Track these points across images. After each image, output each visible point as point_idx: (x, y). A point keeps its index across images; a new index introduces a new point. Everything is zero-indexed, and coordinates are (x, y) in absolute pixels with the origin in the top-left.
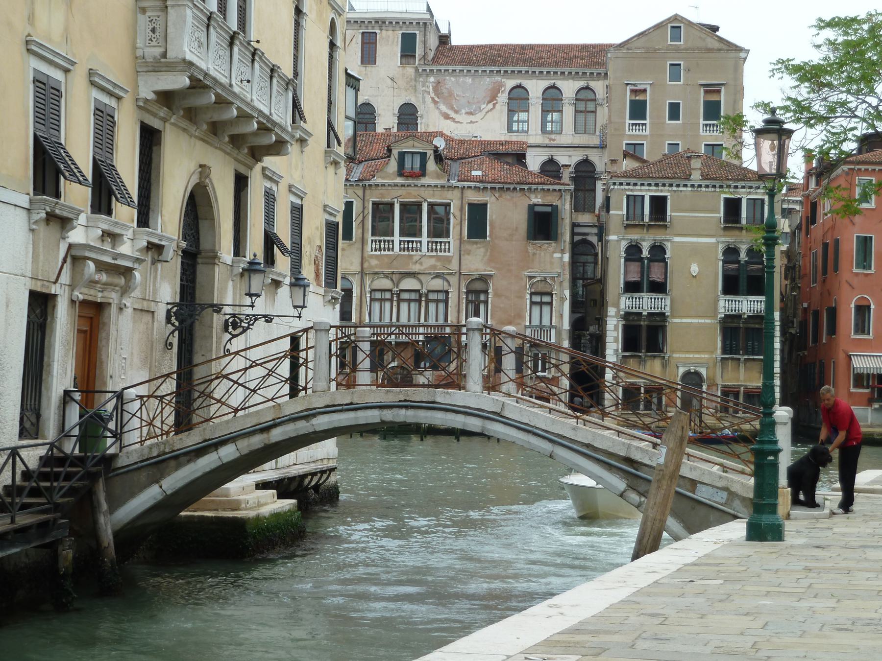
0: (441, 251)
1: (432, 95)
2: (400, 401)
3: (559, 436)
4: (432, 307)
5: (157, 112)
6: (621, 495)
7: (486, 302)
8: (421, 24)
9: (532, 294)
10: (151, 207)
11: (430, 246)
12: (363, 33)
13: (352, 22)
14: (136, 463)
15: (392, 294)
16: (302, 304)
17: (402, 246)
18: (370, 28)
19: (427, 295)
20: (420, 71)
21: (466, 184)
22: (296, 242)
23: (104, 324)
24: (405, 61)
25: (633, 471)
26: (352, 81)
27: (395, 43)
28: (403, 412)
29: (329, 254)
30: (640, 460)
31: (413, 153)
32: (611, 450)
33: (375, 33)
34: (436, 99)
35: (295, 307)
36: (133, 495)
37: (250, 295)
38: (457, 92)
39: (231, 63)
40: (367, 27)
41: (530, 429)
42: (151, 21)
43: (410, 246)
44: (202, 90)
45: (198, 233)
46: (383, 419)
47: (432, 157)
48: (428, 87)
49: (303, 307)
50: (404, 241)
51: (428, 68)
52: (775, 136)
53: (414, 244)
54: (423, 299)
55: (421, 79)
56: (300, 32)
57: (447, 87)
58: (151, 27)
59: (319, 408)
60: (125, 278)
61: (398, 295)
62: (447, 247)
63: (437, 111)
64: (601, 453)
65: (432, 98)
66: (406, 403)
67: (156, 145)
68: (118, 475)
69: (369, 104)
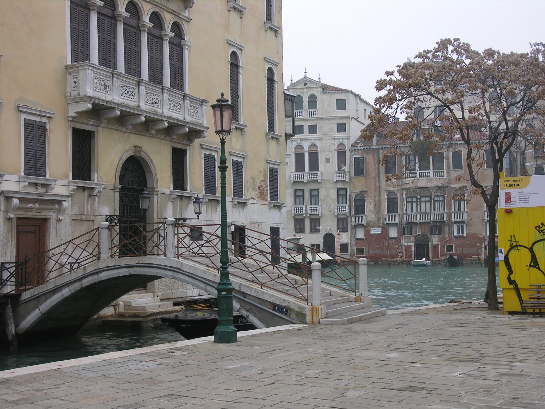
0: (440, 176)
2: (136, 264)
3: (207, 279)
5: (88, 122)
9: (406, 199)
10: (92, 169)
14: (29, 298)
15: (417, 199)
17: (421, 175)
22: (236, 179)
23: (48, 228)
25: (243, 298)
26: (288, 97)
28: (138, 269)
29: (271, 184)
30: (246, 292)
35: (196, 213)
36: (28, 314)
39: (139, 95)
41: (194, 276)
42: (73, 78)
44: (112, 109)
45: (146, 179)
49: (200, 213)
53: (427, 173)
56: (239, 76)
58: (74, 81)
59: (102, 268)
60: (59, 205)
61: (420, 199)
62: (443, 174)
66: (139, 265)
67: (93, 138)
68: (22, 304)
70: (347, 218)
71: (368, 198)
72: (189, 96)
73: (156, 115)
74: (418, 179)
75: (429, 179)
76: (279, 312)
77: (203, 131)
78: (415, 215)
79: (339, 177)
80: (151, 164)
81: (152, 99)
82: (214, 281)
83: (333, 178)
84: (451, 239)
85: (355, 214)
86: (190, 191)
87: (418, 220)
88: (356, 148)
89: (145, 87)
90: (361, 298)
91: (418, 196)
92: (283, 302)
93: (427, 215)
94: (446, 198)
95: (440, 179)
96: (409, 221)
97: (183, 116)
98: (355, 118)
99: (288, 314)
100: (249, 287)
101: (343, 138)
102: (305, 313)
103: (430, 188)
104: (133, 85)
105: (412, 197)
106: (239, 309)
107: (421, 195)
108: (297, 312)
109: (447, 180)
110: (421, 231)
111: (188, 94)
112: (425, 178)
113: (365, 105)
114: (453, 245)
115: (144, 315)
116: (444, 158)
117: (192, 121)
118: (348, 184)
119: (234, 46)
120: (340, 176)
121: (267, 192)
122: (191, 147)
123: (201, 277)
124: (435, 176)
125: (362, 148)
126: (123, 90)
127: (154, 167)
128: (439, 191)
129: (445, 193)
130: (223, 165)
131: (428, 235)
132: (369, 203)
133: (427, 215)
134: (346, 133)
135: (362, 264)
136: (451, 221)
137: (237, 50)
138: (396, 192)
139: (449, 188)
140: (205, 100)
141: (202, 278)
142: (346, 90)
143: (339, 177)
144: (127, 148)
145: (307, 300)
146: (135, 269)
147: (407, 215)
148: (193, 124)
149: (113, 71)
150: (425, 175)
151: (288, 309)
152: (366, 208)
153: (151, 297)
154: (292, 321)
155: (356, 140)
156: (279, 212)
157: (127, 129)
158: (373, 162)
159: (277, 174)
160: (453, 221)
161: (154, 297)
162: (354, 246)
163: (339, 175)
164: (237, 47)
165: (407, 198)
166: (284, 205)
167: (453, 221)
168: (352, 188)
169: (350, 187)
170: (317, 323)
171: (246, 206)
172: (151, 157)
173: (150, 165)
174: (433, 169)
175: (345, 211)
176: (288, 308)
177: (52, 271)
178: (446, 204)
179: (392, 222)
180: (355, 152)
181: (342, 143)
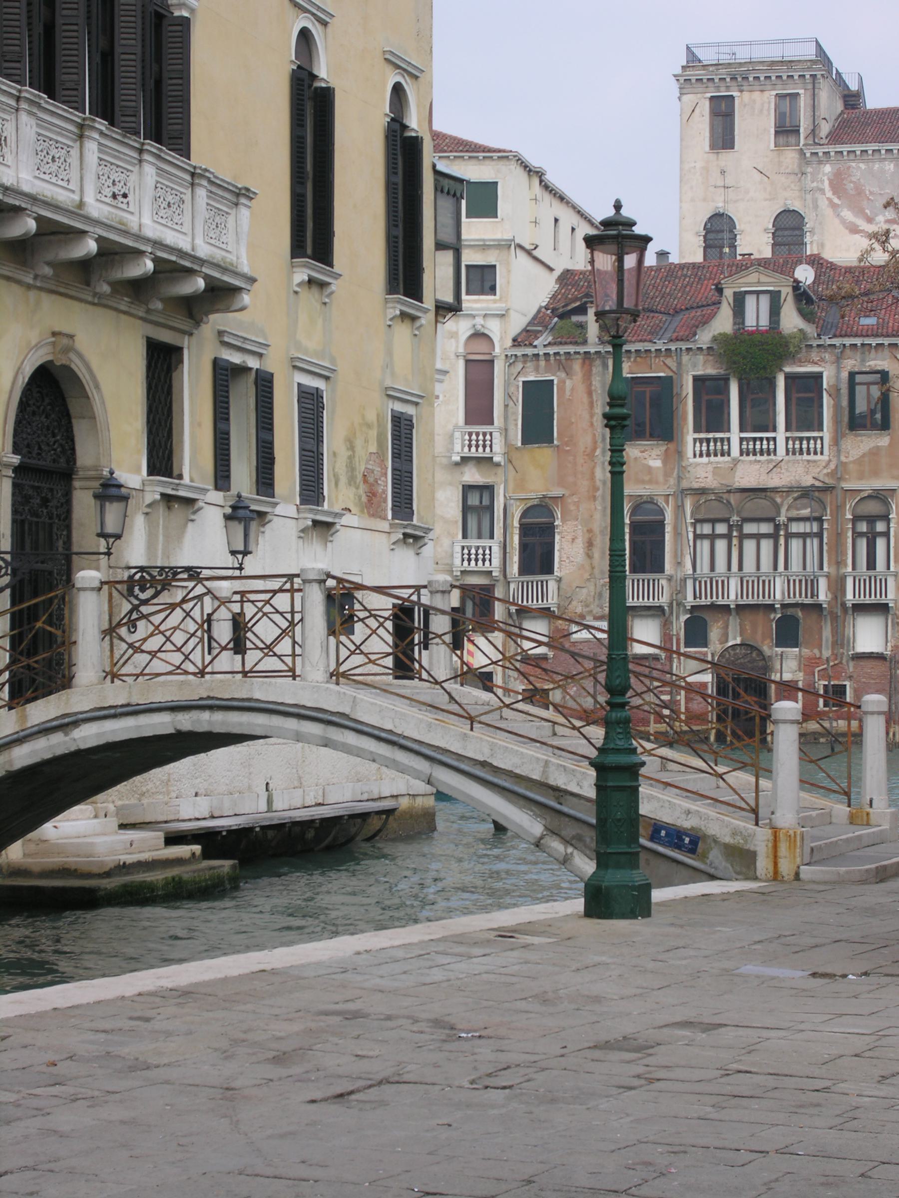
0: (809, 453)
1: (829, 194)
2: (201, 699)
4: (796, 545)
6: (538, 844)
7: (886, 534)
8: (808, 77)
9: (694, 525)
11: (790, 446)
12: (712, 98)
13: (693, 81)
15: (730, 527)
16: (241, 548)
17: (744, 447)
18: (723, 89)
19: (786, 526)
20: (808, 155)
21: (848, 341)
22: (309, 447)
24: (782, 140)
25: (558, 806)
26: (446, 183)
27: (765, 112)
28: (206, 715)
29: (397, 465)
30: (563, 787)
31: (758, 293)
32: (517, 771)
33: (732, 97)
34: (836, 201)
35: (233, 553)
37: (102, 535)
38: (870, 187)
40: (718, 88)
41: (395, 738)
43: (758, 447)
44: (11, 214)
45: (73, 440)
46: (179, 728)
47: (790, 300)
48: (822, 181)
49: (246, 553)
50: (747, 440)
51: (820, 151)
52: (613, 247)
53: (765, 442)
54: (782, 533)
55: (809, 170)
57: (854, 179)
59: (81, 713)
62: (819, 446)
63: (837, 221)
64: (504, 777)
65: (828, 198)
69: (789, 211)
70: (494, 585)
71: (564, 520)
72: (207, 174)
73: (126, 233)
74: (736, 462)
75: (772, 461)
76: (670, 846)
77: (237, 290)
78: (723, 582)
79: (470, 446)
80: (94, 391)
81: (114, 183)
82: (460, 752)
83: (451, 450)
84: (841, 663)
85: (523, 571)
86: (192, 480)
87: (732, 596)
88: (530, 351)
89: (100, 144)
90: (868, 814)
91: (735, 518)
92: (684, 816)
93: (764, 582)
94: (825, 526)
95: (808, 461)
96: (703, 602)
97: (189, 239)
98: (528, 247)
99: (700, 850)
100: (573, 770)
101: (485, 316)
102: (752, 848)
103: (775, 490)
104: (67, 137)
105: (713, 521)
106: (541, 838)
107: (745, 515)
108: (727, 846)
109: (832, 466)
110: (741, 635)
111: (206, 170)
112: (758, 457)
113: (556, 203)
114: (847, 683)
115: (96, 870)
116: (825, 394)
117: (211, 256)
118: (500, 471)
119: (306, 11)
120: (474, 443)
121: (385, 492)
122: (194, 338)
123: (416, 741)
124: (794, 453)
125: (551, 350)
126: (42, 151)
127: (103, 403)
128: (805, 501)
129: (825, 509)
130: (618, 411)
131: (766, 650)
132: (569, 537)
133: (764, 582)
134: (497, 297)
135: (872, 713)
136: (843, 604)
137: (313, 24)
138: (661, 502)
139: (839, 492)
140: (248, 190)
141: (421, 743)
142: (500, 151)
143: (470, 446)
144: (34, 337)
145: (755, 811)
146: (194, 715)
147: (695, 580)
148: (217, 266)
149: (20, 91)
150: (758, 447)
151: (699, 838)
152: (557, 554)
153: (89, 818)
154: (712, 871)
155: (529, 324)
156: (416, 556)
157: (36, 277)
158: (585, 400)
159: (411, 434)
160: (849, 605)
161: (96, 817)
162: (515, 679)
163: (470, 440)
164: (313, 14)
165: (698, 521)
166: (431, 535)
167: (849, 605)
168: (511, 485)
169: (506, 482)
170: (792, 877)
171: (332, 535)
172: (94, 365)
173: (90, 395)
174: (787, 430)
175: (487, 563)
176: (700, 834)
177: (432, 680)
178: (825, 548)
179: (646, 602)
180: (525, 362)
181: (482, 330)
